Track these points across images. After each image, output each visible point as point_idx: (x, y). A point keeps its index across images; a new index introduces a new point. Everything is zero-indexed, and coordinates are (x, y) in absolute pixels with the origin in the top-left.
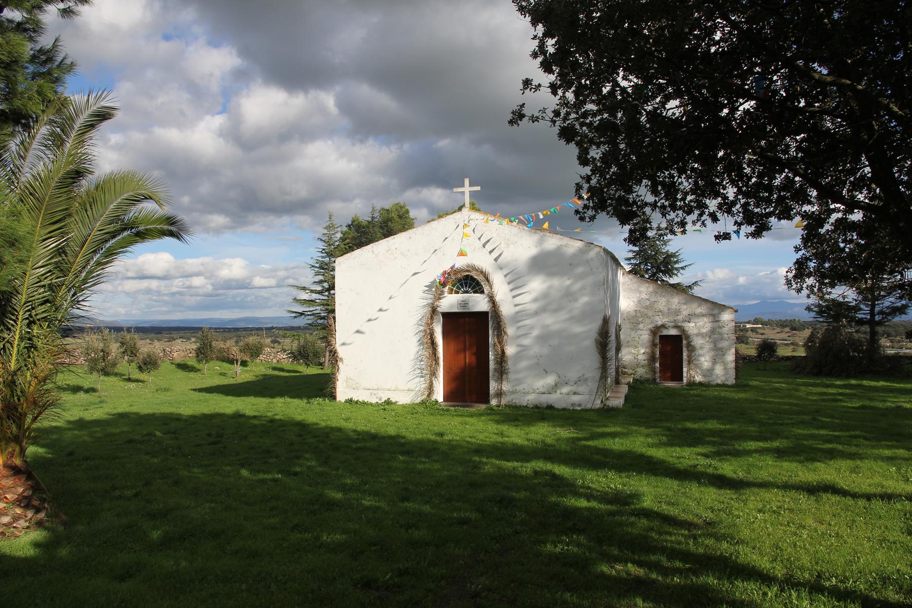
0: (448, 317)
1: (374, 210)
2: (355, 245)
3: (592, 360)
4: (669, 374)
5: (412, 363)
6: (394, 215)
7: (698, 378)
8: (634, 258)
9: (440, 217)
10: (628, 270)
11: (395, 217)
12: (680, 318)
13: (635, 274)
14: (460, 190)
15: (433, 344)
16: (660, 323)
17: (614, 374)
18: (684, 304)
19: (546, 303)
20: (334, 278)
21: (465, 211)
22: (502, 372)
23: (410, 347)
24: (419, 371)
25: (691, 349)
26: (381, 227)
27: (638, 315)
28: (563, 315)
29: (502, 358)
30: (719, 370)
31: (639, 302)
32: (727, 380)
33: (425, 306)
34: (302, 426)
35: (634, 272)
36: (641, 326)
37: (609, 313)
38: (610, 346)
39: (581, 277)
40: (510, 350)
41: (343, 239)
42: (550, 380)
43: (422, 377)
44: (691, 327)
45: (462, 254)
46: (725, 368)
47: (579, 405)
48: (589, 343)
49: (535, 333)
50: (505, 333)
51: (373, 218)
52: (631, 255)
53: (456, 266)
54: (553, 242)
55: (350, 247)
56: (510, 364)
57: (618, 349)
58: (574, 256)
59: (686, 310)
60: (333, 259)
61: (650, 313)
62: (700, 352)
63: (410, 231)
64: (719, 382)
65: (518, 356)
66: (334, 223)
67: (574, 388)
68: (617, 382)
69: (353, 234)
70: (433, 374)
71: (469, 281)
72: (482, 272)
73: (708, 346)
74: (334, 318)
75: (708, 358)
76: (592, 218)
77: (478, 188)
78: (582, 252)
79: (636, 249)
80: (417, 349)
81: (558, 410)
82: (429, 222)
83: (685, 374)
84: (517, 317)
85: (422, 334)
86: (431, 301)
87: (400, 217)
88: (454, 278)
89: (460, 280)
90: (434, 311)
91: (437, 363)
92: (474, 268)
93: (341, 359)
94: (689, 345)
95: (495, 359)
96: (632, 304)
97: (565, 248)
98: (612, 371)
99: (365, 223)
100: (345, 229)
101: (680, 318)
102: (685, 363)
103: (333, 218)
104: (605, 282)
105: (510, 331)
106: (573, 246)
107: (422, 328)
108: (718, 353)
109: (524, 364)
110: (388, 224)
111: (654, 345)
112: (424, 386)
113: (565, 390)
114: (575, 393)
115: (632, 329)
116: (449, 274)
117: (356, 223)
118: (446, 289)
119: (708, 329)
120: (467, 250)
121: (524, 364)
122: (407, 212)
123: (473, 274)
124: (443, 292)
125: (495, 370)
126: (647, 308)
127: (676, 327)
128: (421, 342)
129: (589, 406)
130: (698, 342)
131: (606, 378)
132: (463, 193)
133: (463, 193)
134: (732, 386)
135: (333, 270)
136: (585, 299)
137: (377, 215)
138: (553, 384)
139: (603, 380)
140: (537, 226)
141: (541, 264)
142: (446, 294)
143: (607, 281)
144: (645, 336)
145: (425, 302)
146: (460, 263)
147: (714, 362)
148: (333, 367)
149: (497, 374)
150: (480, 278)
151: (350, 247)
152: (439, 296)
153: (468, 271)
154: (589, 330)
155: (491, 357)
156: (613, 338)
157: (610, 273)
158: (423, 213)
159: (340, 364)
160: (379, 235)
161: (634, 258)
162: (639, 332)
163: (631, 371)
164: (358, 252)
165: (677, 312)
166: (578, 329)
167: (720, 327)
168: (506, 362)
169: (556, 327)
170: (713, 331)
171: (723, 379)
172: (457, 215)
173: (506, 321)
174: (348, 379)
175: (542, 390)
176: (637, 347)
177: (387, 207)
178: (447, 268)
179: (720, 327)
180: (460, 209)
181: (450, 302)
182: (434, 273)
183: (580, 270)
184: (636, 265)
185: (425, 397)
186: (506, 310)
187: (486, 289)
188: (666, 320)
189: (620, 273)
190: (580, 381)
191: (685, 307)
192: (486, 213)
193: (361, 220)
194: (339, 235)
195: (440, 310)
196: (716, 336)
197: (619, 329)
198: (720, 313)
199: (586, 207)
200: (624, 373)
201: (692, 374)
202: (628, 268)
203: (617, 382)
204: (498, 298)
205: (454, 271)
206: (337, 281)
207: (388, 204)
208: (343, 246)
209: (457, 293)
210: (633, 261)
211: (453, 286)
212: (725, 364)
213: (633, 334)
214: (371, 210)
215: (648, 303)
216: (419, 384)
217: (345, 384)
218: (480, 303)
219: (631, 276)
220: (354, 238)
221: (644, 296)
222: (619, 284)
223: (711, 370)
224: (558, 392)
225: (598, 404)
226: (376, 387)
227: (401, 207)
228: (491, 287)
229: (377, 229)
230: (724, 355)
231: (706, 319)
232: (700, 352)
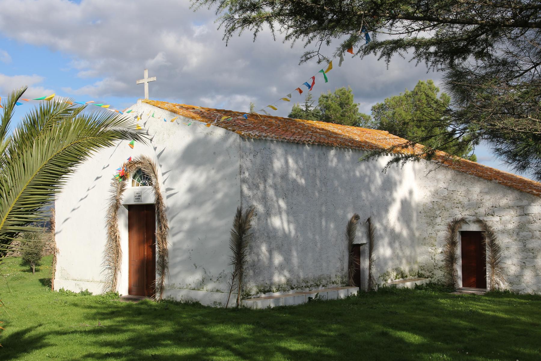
4: (473, 280)
5: (103, 255)
7: (504, 286)
12: (482, 210)
16: (459, 217)
18: (487, 193)
19: (197, 196)
22: (164, 266)
25: (496, 249)
27: (436, 207)
30: (528, 277)
31: (436, 193)
36: (438, 220)
44: (495, 223)
47: (220, 303)
49: (186, 226)
59: (489, 201)
61: (448, 205)
62: (506, 253)
64: (530, 291)
73: (514, 247)
75: (515, 261)
81: (204, 307)
83: (488, 281)
86: (154, 191)
94: (492, 244)
97: (210, 137)
101: (482, 210)
111: (453, 244)
114: (218, 291)
115: (429, 224)
119: (516, 224)
126: (445, 199)
127: (479, 221)
129: (223, 305)
130: (503, 241)
138: (201, 279)
144: (443, 233)
147: (523, 266)
162: (437, 227)
163: (428, 274)
165: (478, 205)
167: (530, 222)
169: (201, 220)
171: (535, 288)
175: (193, 286)
176: (434, 245)
179: (530, 222)
185: (110, 288)
187: (154, 180)
188: (467, 213)
190: (220, 278)
191: (487, 197)
195: (122, 202)
196: (525, 233)
198: (529, 205)
213: (430, 230)
215: (446, 193)
216: (104, 275)
221: (442, 185)
223: (519, 276)
225: (233, 303)
230: (535, 257)
231: (512, 212)
232: (506, 253)
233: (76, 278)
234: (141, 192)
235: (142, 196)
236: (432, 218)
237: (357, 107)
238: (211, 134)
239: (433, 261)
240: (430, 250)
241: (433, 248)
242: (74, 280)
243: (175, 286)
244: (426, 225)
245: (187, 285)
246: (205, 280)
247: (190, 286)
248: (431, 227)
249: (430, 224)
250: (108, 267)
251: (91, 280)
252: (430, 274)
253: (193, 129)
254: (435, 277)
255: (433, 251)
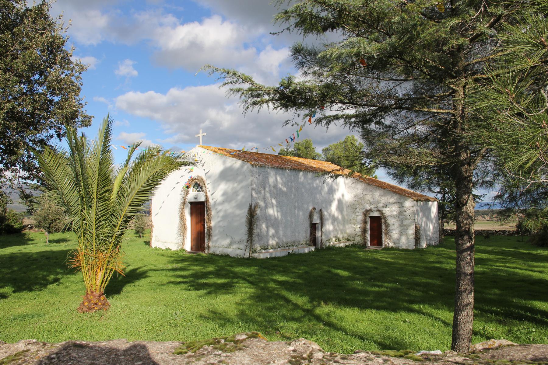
3: (244, 230)
4: (376, 242)
7: (391, 245)
12: (380, 205)
18: (383, 196)
27: (356, 203)
30: (403, 239)
32: (409, 246)
34: (25, 254)
39: (240, 182)
44: (387, 211)
46: (408, 239)
48: (244, 220)
58: (238, 169)
59: (384, 200)
64: (404, 247)
67: (238, 246)
73: (397, 225)
75: (397, 231)
77: (205, 134)
81: (231, 257)
83: (383, 242)
94: (386, 223)
102: (383, 234)
108: (403, 229)
111: (365, 223)
113: (235, 246)
127: (379, 211)
129: (242, 256)
130: (391, 221)
134: (413, 250)
147: (401, 234)
166: (238, 212)
167: (404, 211)
169: (230, 211)
170: (401, 213)
175: (225, 246)
179: (404, 211)
183: (240, 178)
195: (187, 200)
196: (402, 217)
198: (404, 202)
201: (387, 242)
212: (407, 235)
216: (178, 239)
223: (399, 239)
225: (247, 255)
230: (407, 229)
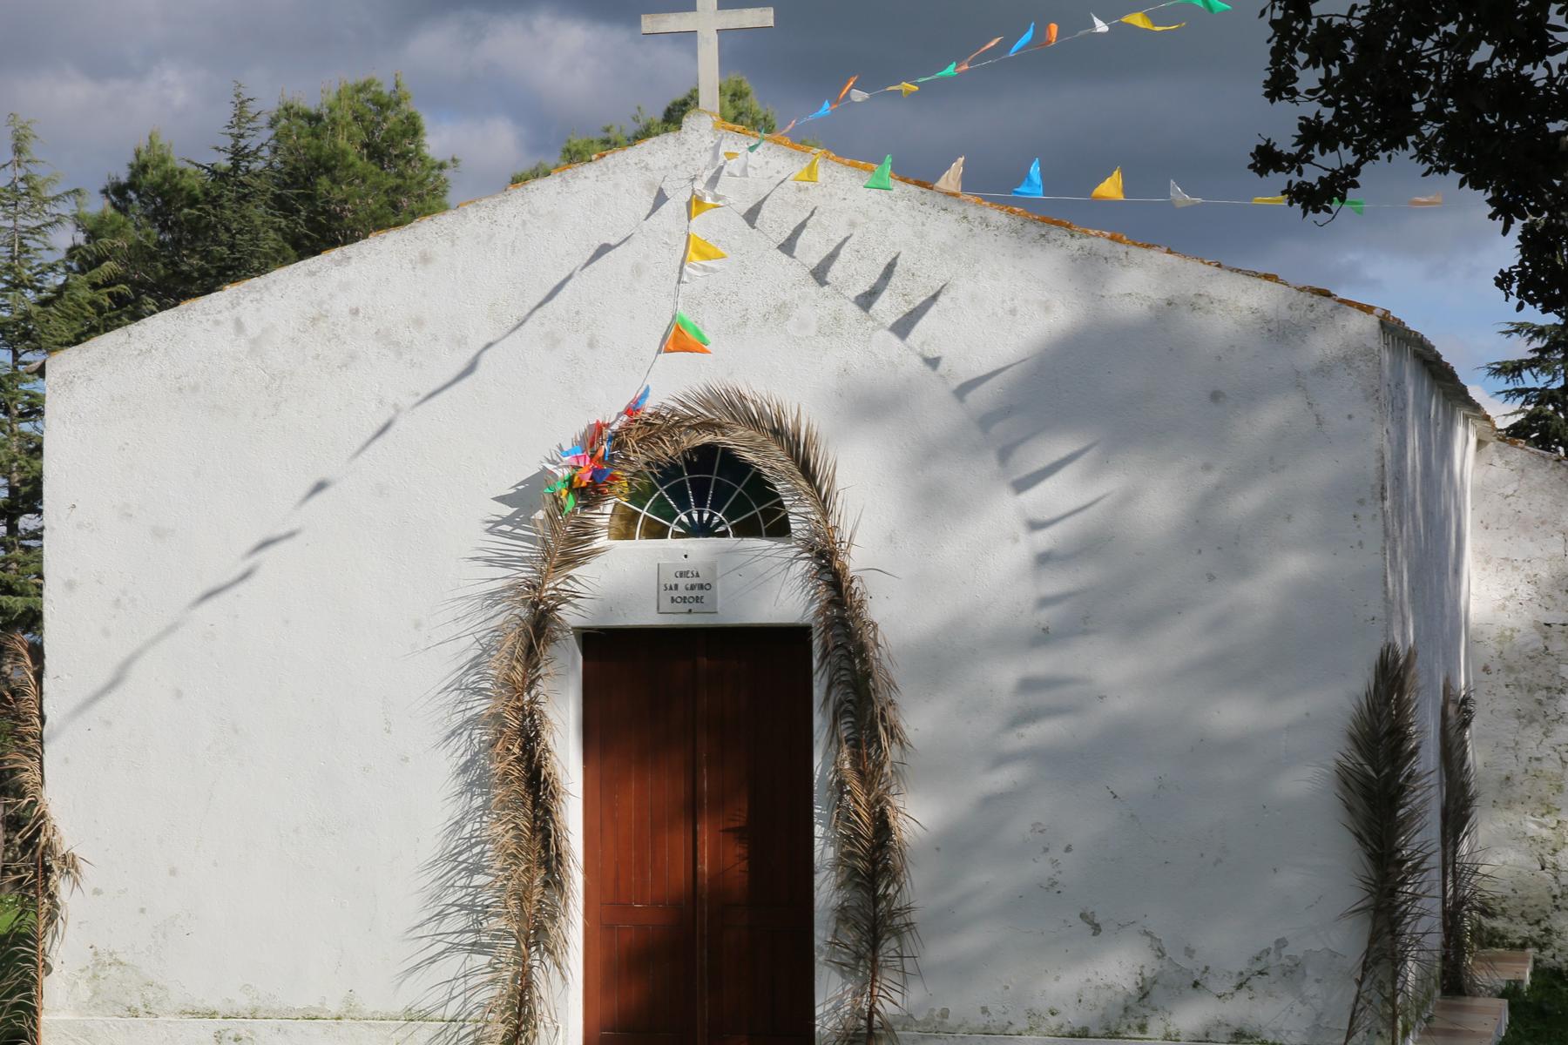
0: (609, 650)
1: (241, 115)
2: (151, 290)
3: (1310, 886)
6: (347, 143)
8: (1539, 362)
9: (575, 156)
10: (1503, 423)
11: (353, 153)
13: (1544, 442)
14: (674, 22)
15: (536, 784)
17: (1435, 941)
19: (1096, 588)
20: (37, 451)
21: (700, 129)
22: (876, 926)
23: (416, 799)
24: (458, 921)
26: (280, 203)
28: (1178, 643)
29: (875, 856)
33: (494, 597)
35: (1535, 432)
37: (1406, 635)
38: (1413, 800)
40: (916, 816)
41: (82, 261)
42: (1117, 968)
43: (477, 948)
45: (678, 340)
48: (1309, 781)
50: (892, 732)
51: (238, 155)
52: (1521, 348)
53: (649, 406)
54: (1140, 281)
55: (120, 300)
56: (917, 889)
57: (1456, 817)
60: (33, 358)
63: (425, 228)
65: (957, 844)
66: (40, 172)
68: (1454, 983)
69: (137, 231)
70: (536, 933)
71: (716, 475)
72: (778, 433)
74: (37, 653)
76: (1337, 186)
77: (762, 17)
78: (1281, 333)
79: (1552, 319)
80: (454, 810)
82: (517, 180)
84: (944, 659)
85: (480, 735)
86: (524, 573)
87: (376, 153)
88: (639, 459)
89: (668, 472)
90: (539, 626)
91: (554, 881)
92: (736, 409)
93: (70, 864)
95: (844, 860)
96: (1525, 591)
98: (1425, 926)
99: (195, 181)
100: (97, 206)
103: (32, 148)
104: (1388, 484)
105: (919, 719)
106: (1236, 301)
107: (480, 706)
109: (990, 879)
110: (315, 190)
112: (485, 995)
116: (618, 441)
117: (153, 176)
118: (604, 514)
120: (706, 322)
121: (990, 879)
122: (412, 128)
123: (737, 440)
124: (585, 531)
125: (843, 915)
128: (474, 777)
131: (1397, 960)
132: (688, 39)
133: (688, 39)
135: (35, 410)
136: (1294, 565)
137: (259, 138)
139: (1381, 972)
140: (1059, 211)
141: (1061, 395)
142: (602, 541)
143: (1400, 477)
145: (499, 577)
146: (672, 385)
148: (27, 905)
149: (850, 937)
150: (770, 462)
151: (120, 300)
152: (569, 548)
153: (709, 426)
154: (1297, 730)
155: (824, 850)
156: (1427, 760)
157: (1413, 441)
158: (500, 141)
159: (62, 887)
160: (271, 240)
161: (1539, 362)
163: (1522, 930)
164: (160, 326)
168: (892, 874)
172: (659, 153)
173: (896, 675)
174: (100, 963)
177: (310, 104)
178: (610, 411)
180: (674, 116)
181: (630, 574)
182: (543, 429)
183: (1272, 415)
184: (1545, 396)
186: (894, 614)
187: (799, 515)
189: (1464, 441)
190: (1267, 970)
192: (800, 141)
193: (176, 162)
194: (66, 237)
195: (571, 616)
197: (1457, 715)
199: (1312, 134)
200: (1493, 939)
202: (1505, 413)
203: (1454, 983)
204: (855, 561)
205: (644, 426)
206: (53, 468)
207: (314, 90)
208: (85, 294)
209: (660, 533)
210: (1529, 380)
211: (638, 498)
213: (1531, 741)
214: (228, 112)
217: (84, 992)
218: (767, 586)
219: (1521, 454)
220: (141, 254)
222: (1457, 495)
224: (1156, 1027)
226: (243, 1002)
227: (382, 106)
228: (823, 504)
229: (257, 213)
233: (214, 1003)
234: (712, 568)
235: (719, 585)
236: (1541, 695)
237: (446, 173)
238: (1194, 307)
239: (1547, 875)
240: (1532, 827)
241: (1547, 819)
242: (195, 1014)
243: (951, 1021)
244: (1515, 723)
245: (1031, 1014)
246: (1156, 991)
247: (1053, 1022)
248: (1535, 732)
249: (1532, 720)
250: (470, 938)
251: (334, 1007)
252: (1536, 932)
253: (1088, 270)
254: (1558, 943)
255: (1545, 833)
